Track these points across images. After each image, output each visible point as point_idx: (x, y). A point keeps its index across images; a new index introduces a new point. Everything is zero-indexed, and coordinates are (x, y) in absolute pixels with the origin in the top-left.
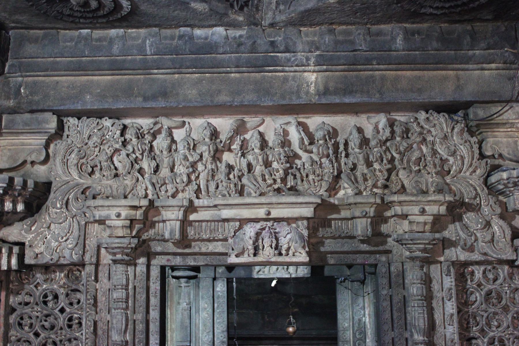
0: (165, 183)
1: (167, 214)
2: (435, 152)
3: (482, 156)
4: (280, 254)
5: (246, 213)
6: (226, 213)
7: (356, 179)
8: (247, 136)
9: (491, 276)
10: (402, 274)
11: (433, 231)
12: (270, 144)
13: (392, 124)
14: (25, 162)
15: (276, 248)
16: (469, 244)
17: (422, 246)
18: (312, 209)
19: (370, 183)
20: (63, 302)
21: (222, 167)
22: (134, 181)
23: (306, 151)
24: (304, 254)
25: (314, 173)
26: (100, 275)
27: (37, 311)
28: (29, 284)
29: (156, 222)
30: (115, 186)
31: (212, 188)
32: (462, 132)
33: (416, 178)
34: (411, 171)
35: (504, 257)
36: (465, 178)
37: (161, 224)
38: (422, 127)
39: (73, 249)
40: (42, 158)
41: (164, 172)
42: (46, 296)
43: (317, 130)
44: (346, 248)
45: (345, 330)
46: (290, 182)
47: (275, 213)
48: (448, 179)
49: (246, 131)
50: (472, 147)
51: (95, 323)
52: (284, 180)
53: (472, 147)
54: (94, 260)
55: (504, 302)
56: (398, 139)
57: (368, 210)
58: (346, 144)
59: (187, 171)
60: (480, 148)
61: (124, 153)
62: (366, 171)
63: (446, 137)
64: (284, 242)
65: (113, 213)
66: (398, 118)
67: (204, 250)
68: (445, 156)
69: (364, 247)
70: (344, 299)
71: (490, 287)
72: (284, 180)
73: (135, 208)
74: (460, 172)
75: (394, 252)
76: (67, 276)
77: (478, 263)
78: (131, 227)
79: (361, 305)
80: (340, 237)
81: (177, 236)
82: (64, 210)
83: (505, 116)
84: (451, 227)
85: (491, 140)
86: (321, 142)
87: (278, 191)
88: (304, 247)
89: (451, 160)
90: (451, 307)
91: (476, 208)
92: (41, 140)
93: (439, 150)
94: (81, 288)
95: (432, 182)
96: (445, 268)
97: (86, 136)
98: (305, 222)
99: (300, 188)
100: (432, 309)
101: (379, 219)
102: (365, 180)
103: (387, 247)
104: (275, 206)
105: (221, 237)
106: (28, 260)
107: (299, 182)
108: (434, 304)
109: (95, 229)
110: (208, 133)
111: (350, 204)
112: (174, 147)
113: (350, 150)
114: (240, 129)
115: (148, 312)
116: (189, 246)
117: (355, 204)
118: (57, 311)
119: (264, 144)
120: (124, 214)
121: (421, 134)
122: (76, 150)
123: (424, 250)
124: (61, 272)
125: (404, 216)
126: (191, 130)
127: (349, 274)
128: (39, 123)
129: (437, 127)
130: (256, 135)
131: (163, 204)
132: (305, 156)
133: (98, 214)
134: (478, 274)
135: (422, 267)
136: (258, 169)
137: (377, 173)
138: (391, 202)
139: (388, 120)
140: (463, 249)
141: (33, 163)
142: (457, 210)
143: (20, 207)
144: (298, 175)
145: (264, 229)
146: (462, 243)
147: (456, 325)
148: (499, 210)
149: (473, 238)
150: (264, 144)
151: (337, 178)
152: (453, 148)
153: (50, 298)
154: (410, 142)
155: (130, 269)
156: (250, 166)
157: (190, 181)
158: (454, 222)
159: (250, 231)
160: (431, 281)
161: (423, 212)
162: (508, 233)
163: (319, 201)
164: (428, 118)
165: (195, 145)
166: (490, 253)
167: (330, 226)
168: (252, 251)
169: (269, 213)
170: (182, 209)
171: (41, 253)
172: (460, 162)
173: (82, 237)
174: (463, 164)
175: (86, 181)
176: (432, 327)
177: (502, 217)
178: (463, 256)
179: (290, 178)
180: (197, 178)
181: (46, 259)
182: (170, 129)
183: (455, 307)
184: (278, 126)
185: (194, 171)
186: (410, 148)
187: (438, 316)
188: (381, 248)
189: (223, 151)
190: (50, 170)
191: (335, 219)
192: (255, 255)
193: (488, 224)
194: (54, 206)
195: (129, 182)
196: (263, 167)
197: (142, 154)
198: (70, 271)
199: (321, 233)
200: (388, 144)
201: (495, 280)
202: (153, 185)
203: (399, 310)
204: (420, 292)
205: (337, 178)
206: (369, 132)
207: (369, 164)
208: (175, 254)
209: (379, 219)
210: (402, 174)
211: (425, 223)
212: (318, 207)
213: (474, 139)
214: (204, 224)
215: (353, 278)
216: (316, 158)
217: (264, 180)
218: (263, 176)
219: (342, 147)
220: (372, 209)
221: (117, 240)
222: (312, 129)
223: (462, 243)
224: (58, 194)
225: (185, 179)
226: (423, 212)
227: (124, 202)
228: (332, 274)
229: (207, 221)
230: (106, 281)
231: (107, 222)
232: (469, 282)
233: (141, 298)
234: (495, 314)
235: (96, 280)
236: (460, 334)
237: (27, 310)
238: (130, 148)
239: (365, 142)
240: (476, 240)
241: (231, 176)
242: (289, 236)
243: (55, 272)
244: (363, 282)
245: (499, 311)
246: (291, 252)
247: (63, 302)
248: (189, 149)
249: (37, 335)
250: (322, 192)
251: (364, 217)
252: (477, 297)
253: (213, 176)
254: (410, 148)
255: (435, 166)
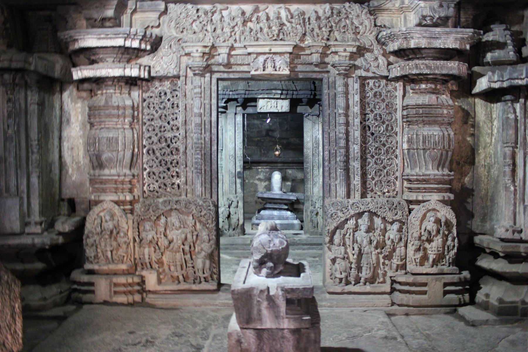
0: (218, 37)
1: (220, 51)
2: (352, 23)
3: (375, 25)
4: (276, 70)
5: (260, 50)
6: (250, 50)
7: (313, 36)
8: (260, 14)
9: (377, 85)
10: (335, 82)
11: (350, 60)
12: (271, 18)
13: (332, 9)
14: (148, 27)
15: (274, 67)
16: (367, 67)
17: (344, 68)
18: (292, 48)
19: (320, 38)
20: (169, 96)
21: (248, 29)
22: (204, 35)
23: (289, 22)
24: (288, 70)
25: (293, 32)
26: (187, 82)
27: (157, 100)
28: (152, 87)
29: (215, 55)
30: (194, 38)
31: (242, 39)
32: (366, 13)
33: (343, 35)
34: (340, 32)
35: (383, 74)
36: (367, 36)
37: (217, 57)
38: (347, 11)
39: (174, 69)
40: (157, 24)
41: (219, 31)
42: (160, 93)
43: (295, 11)
44: (308, 70)
45: (308, 142)
46: (281, 36)
47: (274, 50)
48: (359, 37)
49: (259, 12)
50: (371, 21)
51: (186, 105)
52: (278, 35)
53: (371, 21)
54: (184, 74)
55: (382, 97)
56: (335, 16)
57: (318, 49)
58: (309, 18)
59: (230, 30)
60: (375, 22)
61: (198, 22)
62: (318, 32)
63: (358, 16)
64: (278, 65)
65: (194, 50)
66: (335, 7)
67: (238, 70)
68: (357, 25)
69: (317, 69)
70: (308, 125)
71: (377, 90)
72: (278, 35)
73: (205, 47)
74: (364, 33)
75: (331, 72)
76: (171, 83)
77: (371, 78)
78: (203, 57)
79: (317, 128)
80: (305, 64)
81: (226, 61)
82: (169, 49)
83: (387, 6)
84: (359, 60)
85: (380, 18)
86: (297, 17)
87: (275, 40)
88: (287, 67)
89: (360, 27)
90: (357, 98)
91: (371, 51)
92: (157, 15)
93: (355, 22)
94: (178, 89)
95: (351, 37)
96: (355, 79)
97: (179, 13)
98: (288, 55)
99: (286, 39)
100: (348, 99)
101: (324, 55)
102: (318, 36)
103: (327, 70)
104: (274, 46)
105: (247, 63)
106: (153, 74)
107: (285, 36)
108: (349, 97)
109: (185, 59)
110: (240, 12)
111: (309, 47)
112: (223, 20)
113: (311, 22)
114: (256, 10)
115: (211, 100)
116: (231, 68)
117: (313, 46)
118: (166, 100)
119: (268, 18)
120: (200, 50)
121: (346, 14)
122: (174, 21)
123: (345, 70)
124: (168, 81)
125: (336, 53)
126: (231, 11)
127: (310, 111)
128: (156, 6)
129: (355, 10)
130: (264, 14)
131: (219, 45)
132: (288, 24)
133: (187, 50)
134: (371, 84)
135: (344, 79)
136: (265, 30)
137: (324, 33)
138: (329, 45)
139: (331, 7)
140: (364, 70)
141: (152, 27)
142: (361, 51)
143: (149, 48)
144: (285, 33)
145: (268, 58)
146: (363, 67)
147: (359, 106)
148: (382, 52)
149: (369, 65)
150: (268, 18)
151: (304, 35)
152: (361, 21)
153: (163, 94)
154: (341, 18)
155: (202, 79)
156: (261, 29)
157: (231, 36)
158: (360, 57)
159: (261, 59)
160: (348, 86)
161: (345, 50)
162: (386, 63)
163: (295, 44)
164: (350, 6)
165: (233, 18)
166: (377, 72)
167: (300, 58)
168: (262, 69)
169: (271, 50)
170: (228, 48)
171: (159, 71)
172: (364, 28)
173: (179, 63)
174: (366, 29)
175: (180, 36)
176: (347, 107)
177: (383, 55)
178: (364, 74)
179: (281, 34)
180: (235, 34)
181: (161, 73)
182: (221, 10)
183: (359, 98)
184: (275, 9)
185: (233, 31)
186: (340, 20)
187: (351, 103)
188: (325, 70)
189: (247, 22)
190: (161, 30)
191: (303, 55)
192: (264, 70)
193: (376, 59)
194: (164, 49)
195: (201, 36)
196: (268, 29)
197: (207, 22)
198: (172, 81)
199: (296, 61)
200: (330, 19)
201: (379, 86)
202: (213, 37)
203: (332, 99)
204: (342, 90)
205: (304, 35)
206: (321, 13)
207: (320, 28)
208: (224, 72)
209: (324, 55)
210: (336, 34)
211: (346, 56)
212: (295, 47)
213: (372, 17)
214: (238, 57)
215: (313, 114)
216: (294, 25)
217: (268, 35)
218: (268, 33)
219: (307, 20)
220: (321, 49)
221: (196, 63)
222: (292, 11)
223: (363, 67)
224: (166, 42)
225: (229, 34)
226: (345, 50)
227: (200, 44)
228: (301, 112)
229: (240, 55)
230: (190, 84)
231: (191, 54)
232: (367, 87)
233: (208, 93)
234: (378, 102)
235: (186, 84)
236: (361, 112)
237: (152, 100)
238: (201, 19)
239: (318, 18)
240: (370, 66)
241: (252, 33)
242: (280, 62)
243: (165, 81)
244: (318, 116)
245: (380, 101)
246: (281, 70)
247: (169, 96)
248: (231, 19)
249: (157, 112)
250: (297, 41)
251: (317, 53)
252: (370, 94)
253: (243, 33)
254: (340, 20)
255: (352, 30)
